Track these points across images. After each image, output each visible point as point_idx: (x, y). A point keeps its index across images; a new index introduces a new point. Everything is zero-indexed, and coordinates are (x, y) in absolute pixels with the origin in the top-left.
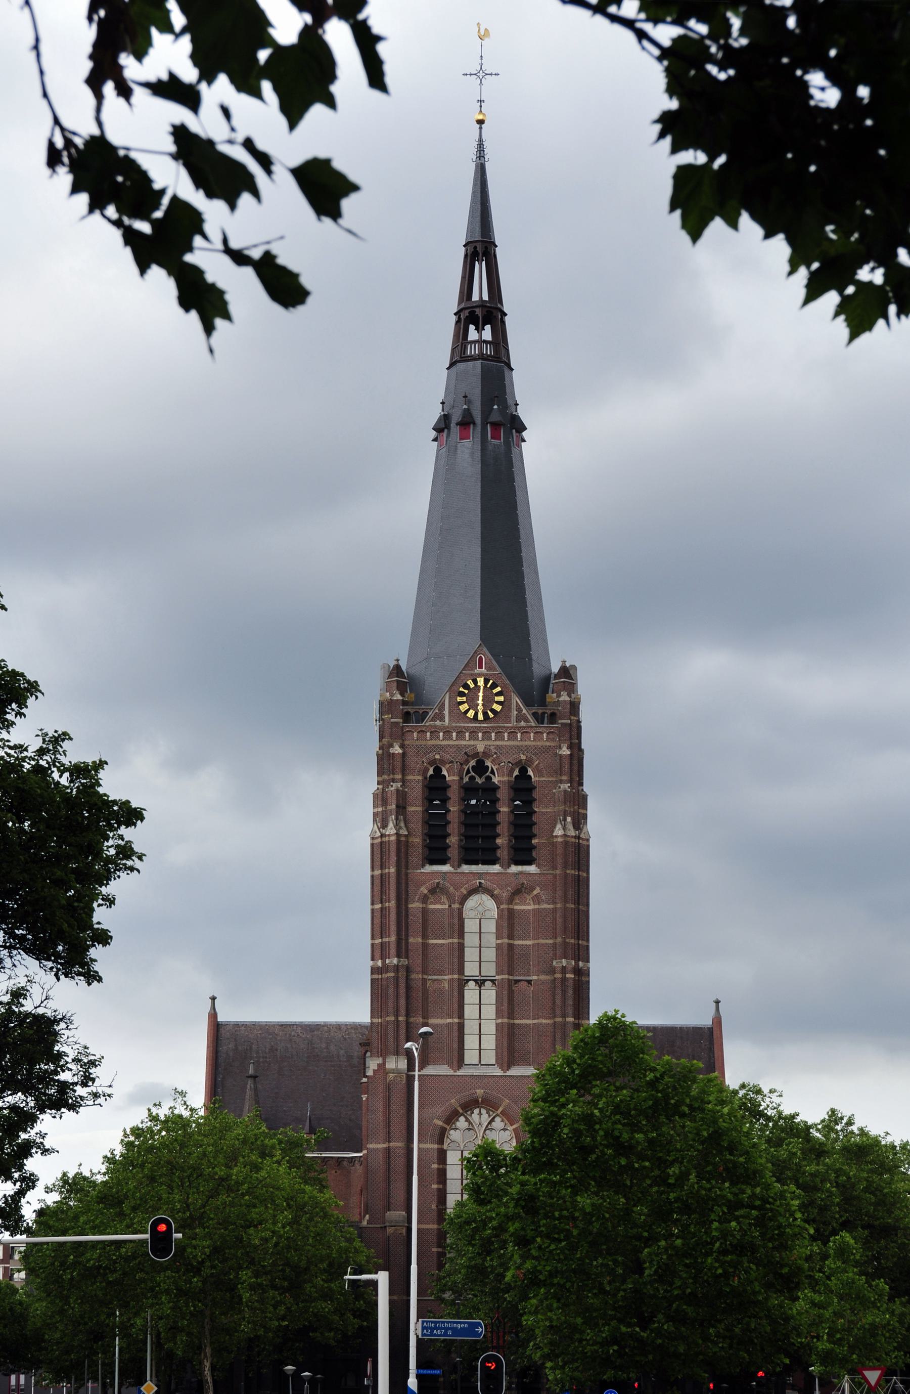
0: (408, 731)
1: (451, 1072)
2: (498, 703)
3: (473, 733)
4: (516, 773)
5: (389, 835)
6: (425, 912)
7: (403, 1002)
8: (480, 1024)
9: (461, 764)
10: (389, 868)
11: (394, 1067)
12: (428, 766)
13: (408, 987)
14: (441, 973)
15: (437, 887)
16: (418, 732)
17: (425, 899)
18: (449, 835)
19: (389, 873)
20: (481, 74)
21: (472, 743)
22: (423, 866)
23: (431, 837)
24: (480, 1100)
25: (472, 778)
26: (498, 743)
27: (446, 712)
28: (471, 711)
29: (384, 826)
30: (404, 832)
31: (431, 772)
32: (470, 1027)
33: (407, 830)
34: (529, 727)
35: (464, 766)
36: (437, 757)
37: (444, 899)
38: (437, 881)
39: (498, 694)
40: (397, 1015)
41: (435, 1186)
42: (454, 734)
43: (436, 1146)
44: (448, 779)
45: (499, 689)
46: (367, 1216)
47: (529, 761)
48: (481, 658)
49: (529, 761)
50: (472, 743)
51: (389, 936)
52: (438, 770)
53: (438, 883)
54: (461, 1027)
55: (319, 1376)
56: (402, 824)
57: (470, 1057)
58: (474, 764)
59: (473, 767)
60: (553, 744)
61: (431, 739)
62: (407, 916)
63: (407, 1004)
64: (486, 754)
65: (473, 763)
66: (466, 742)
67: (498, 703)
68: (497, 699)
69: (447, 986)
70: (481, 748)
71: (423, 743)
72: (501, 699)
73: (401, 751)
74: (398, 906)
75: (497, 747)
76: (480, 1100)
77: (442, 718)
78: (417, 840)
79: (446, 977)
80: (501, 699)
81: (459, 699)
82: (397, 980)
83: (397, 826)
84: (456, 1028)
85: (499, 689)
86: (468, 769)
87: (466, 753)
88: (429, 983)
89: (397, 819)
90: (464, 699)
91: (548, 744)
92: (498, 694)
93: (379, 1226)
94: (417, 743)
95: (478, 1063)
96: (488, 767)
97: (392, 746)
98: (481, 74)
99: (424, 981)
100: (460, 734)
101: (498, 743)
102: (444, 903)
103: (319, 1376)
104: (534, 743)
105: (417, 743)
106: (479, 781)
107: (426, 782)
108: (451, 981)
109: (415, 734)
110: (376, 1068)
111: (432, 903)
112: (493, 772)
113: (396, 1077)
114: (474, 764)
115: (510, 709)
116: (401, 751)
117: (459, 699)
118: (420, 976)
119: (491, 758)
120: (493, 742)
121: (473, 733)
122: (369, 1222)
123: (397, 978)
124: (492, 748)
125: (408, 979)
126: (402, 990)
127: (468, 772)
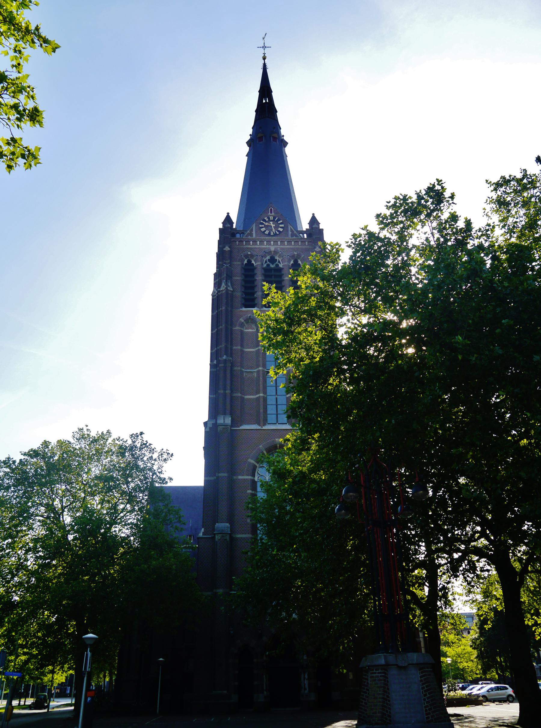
0: (233, 241)
1: (260, 428)
2: (281, 227)
3: (269, 242)
4: (292, 262)
5: (222, 291)
6: (242, 332)
7: (228, 382)
8: (277, 398)
9: (262, 257)
10: (222, 308)
11: (222, 422)
12: (244, 258)
13: (232, 375)
14: (252, 368)
15: (250, 318)
16: (239, 242)
17: (242, 325)
18: (256, 292)
19: (221, 310)
20: (264, 47)
21: (268, 246)
22: (241, 308)
23: (246, 293)
24: (278, 446)
25: (268, 265)
26: (282, 247)
27: (254, 232)
28: (264, 228)
29: (219, 287)
30: (230, 289)
31: (246, 262)
32: (271, 400)
33: (233, 288)
34: (297, 239)
35: (264, 258)
36: (249, 253)
37: (253, 326)
38: (250, 315)
39: (281, 223)
40: (225, 389)
41: (249, 491)
42: (258, 242)
43: (250, 477)
44: (255, 265)
45: (281, 221)
46: (203, 529)
47: (299, 256)
48: (271, 209)
49: (299, 256)
50: (268, 246)
51: (221, 345)
52: (249, 261)
53: (250, 316)
54: (265, 400)
55: (161, 659)
56: (229, 284)
57: (271, 418)
58: (269, 258)
59: (269, 260)
60: (311, 247)
61: (246, 245)
62: (231, 334)
63: (231, 407)
64: (276, 252)
65: (268, 257)
66: (265, 246)
67: (281, 227)
68: (281, 226)
69: (256, 375)
70: (272, 249)
71: (242, 247)
72: (283, 226)
73: (229, 249)
74: (226, 328)
75: (281, 248)
76: (278, 446)
77: (251, 235)
78: (239, 294)
79: (255, 370)
80: (283, 226)
81: (260, 226)
82: (217, 306)
83: (226, 284)
84: (262, 400)
85: (281, 221)
86: (266, 260)
87: (264, 251)
88: (244, 374)
89: (226, 281)
90: (263, 226)
91: (308, 247)
92: (281, 223)
93: (210, 536)
94: (238, 247)
95: (275, 422)
96: (276, 260)
97: (225, 247)
98: (264, 47)
99: (242, 372)
100: (262, 242)
101: (282, 247)
102: (253, 329)
103: (161, 659)
104: (300, 247)
105: (238, 247)
106: (272, 266)
107: (243, 266)
108: (258, 371)
109: (237, 242)
110: (211, 426)
111: (246, 329)
112: (279, 262)
113: (224, 428)
114: (269, 258)
115: (288, 231)
116: (229, 249)
117: (260, 226)
118: (239, 368)
119: (278, 254)
120: (279, 246)
121: (269, 242)
122: (204, 534)
123: (225, 367)
124: (278, 249)
125: (232, 370)
126: (228, 375)
127: (266, 262)
